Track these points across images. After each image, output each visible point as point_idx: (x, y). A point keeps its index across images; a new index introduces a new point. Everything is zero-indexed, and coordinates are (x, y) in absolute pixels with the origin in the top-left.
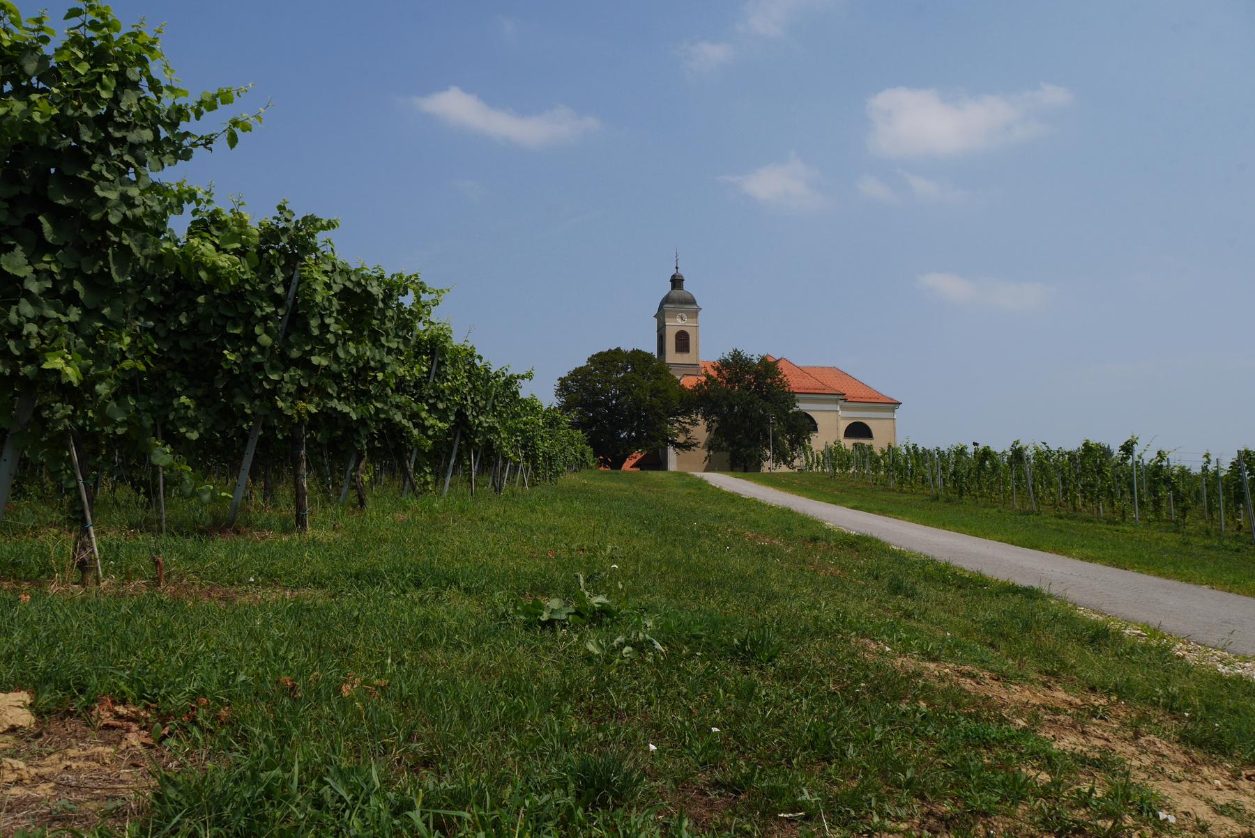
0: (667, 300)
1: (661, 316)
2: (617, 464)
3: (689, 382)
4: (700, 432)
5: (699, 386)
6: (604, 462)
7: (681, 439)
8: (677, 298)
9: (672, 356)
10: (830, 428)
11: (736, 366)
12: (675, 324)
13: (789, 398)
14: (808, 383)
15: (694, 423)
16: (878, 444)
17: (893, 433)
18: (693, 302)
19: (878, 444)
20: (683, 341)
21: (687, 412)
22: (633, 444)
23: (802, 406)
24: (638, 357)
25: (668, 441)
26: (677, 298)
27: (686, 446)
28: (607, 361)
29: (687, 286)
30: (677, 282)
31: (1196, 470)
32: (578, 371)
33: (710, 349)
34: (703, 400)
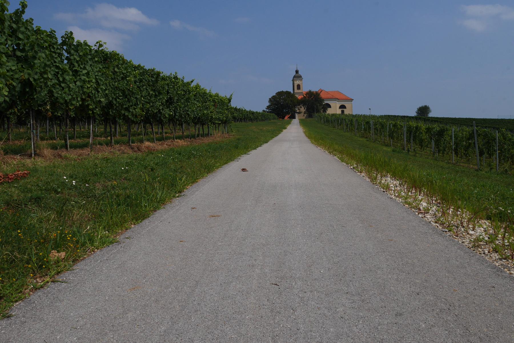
0: (294, 77)
1: (293, 80)
2: (283, 118)
3: (299, 97)
4: (303, 110)
5: (302, 99)
6: (280, 118)
7: (298, 111)
8: (297, 76)
9: (296, 91)
10: (334, 109)
11: (310, 94)
12: (297, 82)
13: (322, 100)
14: (329, 96)
15: (301, 107)
16: (346, 112)
17: (355, 109)
18: (301, 77)
19: (346, 112)
20: (299, 87)
21: (299, 105)
22: (288, 113)
23: (326, 102)
24: (288, 93)
25: (295, 112)
26: (297, 76)
27: (299, 113)
28: (280, 94)
29: (299, 73)
30: (297, 72)
31: (208, 92)
32: (273, 96)
33: (305, 89)
34: (303, 102)
